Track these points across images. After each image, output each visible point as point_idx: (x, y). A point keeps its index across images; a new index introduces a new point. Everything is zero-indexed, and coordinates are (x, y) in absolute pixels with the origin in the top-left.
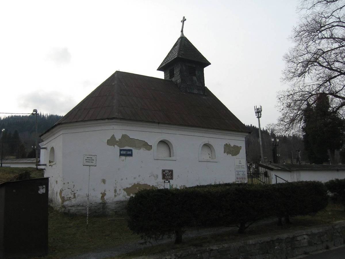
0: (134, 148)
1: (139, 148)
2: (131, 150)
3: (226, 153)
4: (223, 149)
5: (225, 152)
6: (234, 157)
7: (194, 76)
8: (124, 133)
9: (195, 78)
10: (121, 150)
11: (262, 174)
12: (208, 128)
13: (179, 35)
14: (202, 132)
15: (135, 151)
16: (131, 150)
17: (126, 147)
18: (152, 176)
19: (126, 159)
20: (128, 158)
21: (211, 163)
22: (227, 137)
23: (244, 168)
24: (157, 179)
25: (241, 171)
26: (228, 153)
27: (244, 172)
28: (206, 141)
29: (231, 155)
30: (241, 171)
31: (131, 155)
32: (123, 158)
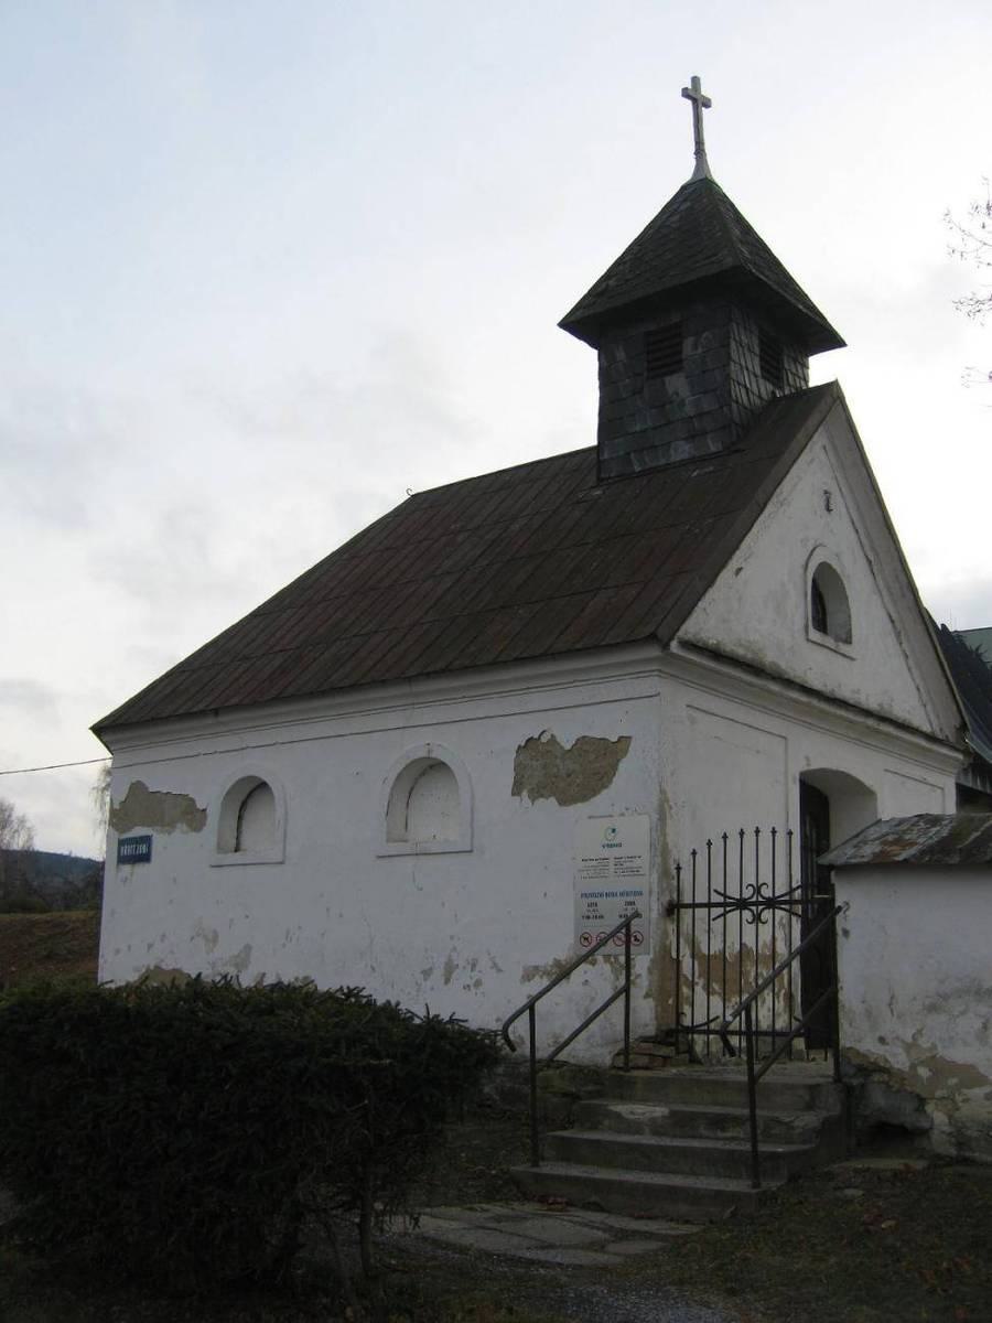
0: (158, 828)
1: (168, 825)
2: (147, 840)
3: (525, 793)
4: (512, 774)
5: (516, 791)
6: (580, 808)
7: (666, 374)
8: (529, 728)
9: (677, 384)
10: (121, 843)
11: (709, 905)
12: (473, 668)
13: (684, 173)
14: (250, 725)
15: (160, 841)
16: (147, 840)
17: (137, 828)
18: (198, 935)
19: (132, 874)
20: (141, 869)
21: (431, 857)
22: (537, 700)
23: (635, 872)
24: (212, 951)
25: (614, 895)
26: (536, 794)
27: (630, 899)
28: (414, 745)
29: (553, 800)
30: (614, 895)
31: (146, 858)
32: (127, 868)
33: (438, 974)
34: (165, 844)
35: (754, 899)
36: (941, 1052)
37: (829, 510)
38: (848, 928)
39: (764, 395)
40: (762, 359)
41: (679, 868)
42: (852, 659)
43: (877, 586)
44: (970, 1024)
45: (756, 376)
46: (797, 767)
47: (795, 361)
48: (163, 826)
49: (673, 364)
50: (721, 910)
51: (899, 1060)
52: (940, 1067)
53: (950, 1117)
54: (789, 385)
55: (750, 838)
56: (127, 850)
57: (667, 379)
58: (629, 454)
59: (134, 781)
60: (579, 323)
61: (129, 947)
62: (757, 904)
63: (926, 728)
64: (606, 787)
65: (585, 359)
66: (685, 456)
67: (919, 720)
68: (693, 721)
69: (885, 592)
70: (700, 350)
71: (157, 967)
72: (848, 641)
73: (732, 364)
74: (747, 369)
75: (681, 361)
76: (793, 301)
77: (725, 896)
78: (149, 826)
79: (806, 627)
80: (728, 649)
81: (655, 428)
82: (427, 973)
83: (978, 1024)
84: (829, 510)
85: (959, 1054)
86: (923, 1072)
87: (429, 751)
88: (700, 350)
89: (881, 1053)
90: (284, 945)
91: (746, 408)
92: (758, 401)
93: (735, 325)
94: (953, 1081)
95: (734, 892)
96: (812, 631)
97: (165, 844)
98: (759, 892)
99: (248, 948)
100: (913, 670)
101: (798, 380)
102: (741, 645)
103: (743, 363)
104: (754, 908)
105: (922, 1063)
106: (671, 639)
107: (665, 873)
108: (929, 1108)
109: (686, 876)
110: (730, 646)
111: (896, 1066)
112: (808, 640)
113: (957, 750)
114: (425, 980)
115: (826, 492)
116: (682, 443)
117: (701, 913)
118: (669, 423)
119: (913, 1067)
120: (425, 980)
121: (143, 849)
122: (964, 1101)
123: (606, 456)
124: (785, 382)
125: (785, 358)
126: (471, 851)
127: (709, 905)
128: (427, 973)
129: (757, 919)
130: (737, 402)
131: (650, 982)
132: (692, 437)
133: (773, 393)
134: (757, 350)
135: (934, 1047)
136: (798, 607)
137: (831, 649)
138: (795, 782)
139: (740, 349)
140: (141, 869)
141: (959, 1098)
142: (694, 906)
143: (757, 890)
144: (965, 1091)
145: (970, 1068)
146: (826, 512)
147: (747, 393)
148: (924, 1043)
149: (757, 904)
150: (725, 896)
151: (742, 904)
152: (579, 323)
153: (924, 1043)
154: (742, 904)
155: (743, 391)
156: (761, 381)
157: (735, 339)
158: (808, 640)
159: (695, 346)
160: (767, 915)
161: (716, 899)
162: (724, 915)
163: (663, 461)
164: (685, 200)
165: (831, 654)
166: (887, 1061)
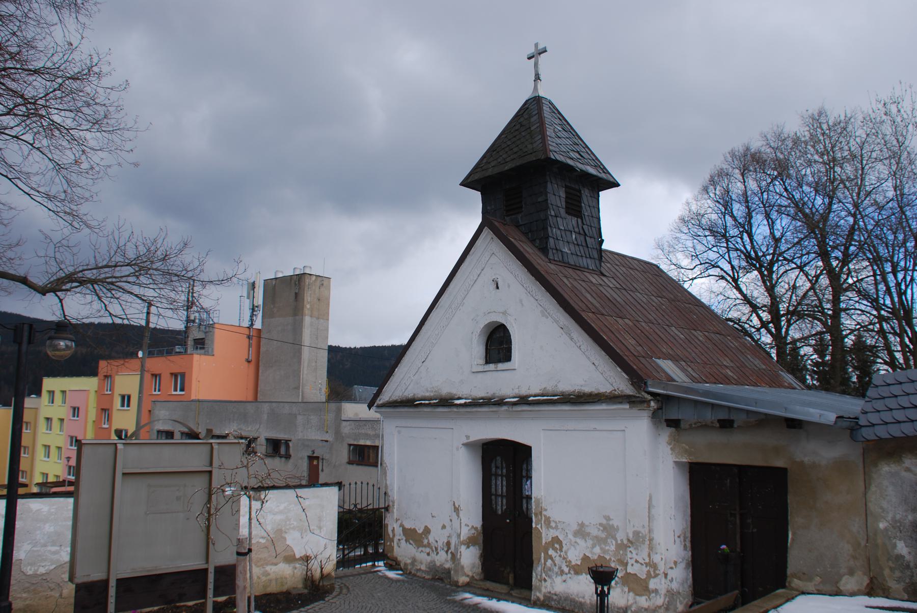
60: (468, 183)
98: (356, 507)
165: (494, 373)
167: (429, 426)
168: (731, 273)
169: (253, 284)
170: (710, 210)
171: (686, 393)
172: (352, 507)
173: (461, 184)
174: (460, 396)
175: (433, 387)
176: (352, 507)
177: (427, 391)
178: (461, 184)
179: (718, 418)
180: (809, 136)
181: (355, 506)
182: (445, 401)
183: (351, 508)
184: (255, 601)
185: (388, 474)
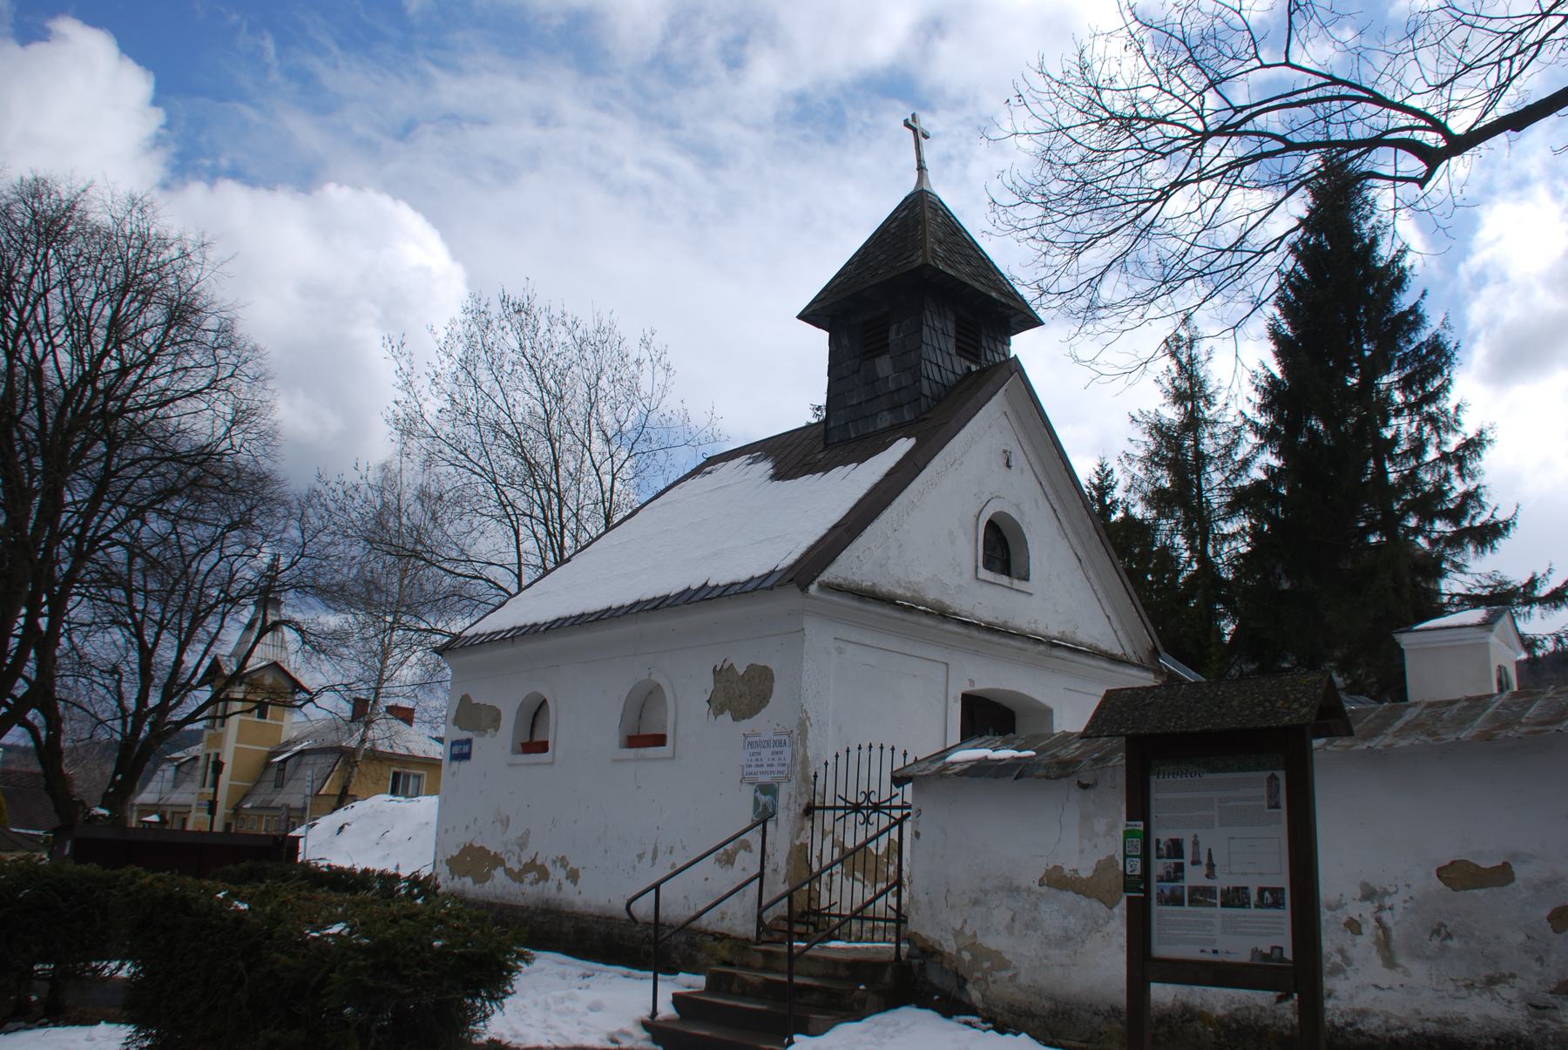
0: (476, 732)
2: (469, 742)
9: (884, 366)
11: (835, 808)
13: (908, 186)
16: (469, 742)
32: (456, 764)
33: (649, 856)
34: (482, 745)
35: (865, 804)
36: (980, 940)
37: (1008, 466)
38: (920, 831)
39: (958, 370)
40: (957, 340)
41: (816, 776)
42: (1031, 594)
43: (1064, 530)
44: (1001, 917)
45: (950, 355)
46: (959, 687)
47: (995, 339)
48: (479, 730)
49: (881, 347)
50: (842, 812)
51: (950, 946)
52: (979, 953)
53: (983, 996)
54: (986, 360)
55: (876, 751)
56: (456, 750)
57: (877, 360)
58: (847, 423)
59: (760, 662)
60: (810, 315)
61: (454, 828)
62: (867, 808)
63: (1117, 651)
64: (764, 706)
65: (819, 339)
66: (887, 424)
67: (1110, 644)
68: (840, 651)
69: (1070, 535)
70: (901, 335)
71: (471, 845)
72: (1026, 578)
73: (924, 346)
74: (940, 349)
75: (888, 345)
76: (983, 289)
77: (845, 800)
78: (470, 731)
79: (977, 567)
80: (884, 590)
81: (867, 401)
82: (640, 857)
83: (1008, 916)
84: (1008, 466)
85: (992, 942)
86: (966, 956)
87: (650, 674)
88: (901, 335)
89: (937, 938)
90: (550, 830)
91: (937, 382)
92: (951, 376)
93: (928, 314)
94: (987, 965)
95: (852, 798)
96: (982, 570)
97: (482, 745)
98: (869, 800)
99: (528, 831)
100: (1103, 601)
101: (996, 356)
102: (900, 586)
103: (936, 345)
104: (865, 812)
105: (966, 948)
106: (811, 582)
107: (805, 779)
108: (969, 987)
109: (820, 781)
110: (886, 586)
111: (947, 950)
112: (977, 579)
113: (1147, 669)
114: (639, 862)
115: (1005, 452)
116: (885, 413)
117: (829, 814)
118: (878, 397)
119: (959, 951)
120: (639, 862)
121: (466, 749)
122: (994, 982)
123: (832, 425)
124: (983, 357)
125: (983, 337)
126: (552, 763)
127: (835, 808)
128: (640, 857)
129: (867, 820)
130: (928, 378)
131: (788, 870)
132: (893, 409)
133: (969, 368)
134: (952, 333)
135: (975, 935)
136: (969, 549)
137: (990, 583)
138: (956, 701)
139: (933, 332)
140: (465, 764)
141: (990, 979)
142: (824, 808)
143: (868, 797)
144: (994, 973)
145: (998, 954)
146: (1004, 469)
147: (940, 370)
148: (968, 931)
149: (867, 808)
150: (845, 800)
151: (857, 808)
152: (810, 315)
153: (968, 931)
154: (857, 808)
155: (935, 369)
156: (956, 359)
157: (927, 325)
158: (977, 579)
159: (898, 333)
160: (874, 817)
161: (840, 803)
162: (844, 816)
163: (871, 430)
164: (904, 210)
165: (1006, 590)
166: (941, 945)
167: (868, 642)
168: (1249, 126)
169: (951, 533)
170: (1252, 439)
171: (1278, 786)
172: (861, 798)
173: (802, 317)
174: (957, 611)
175: (910, 582)
176: (861, 798)
177: (900, 586)
178: (802, 317)
179: (1026, 583)
180: (1290, 268)
181: (868, 797)
182: (942, 614)
183: (860, 801)
184: (1222, 895)
185: (810, 736)
